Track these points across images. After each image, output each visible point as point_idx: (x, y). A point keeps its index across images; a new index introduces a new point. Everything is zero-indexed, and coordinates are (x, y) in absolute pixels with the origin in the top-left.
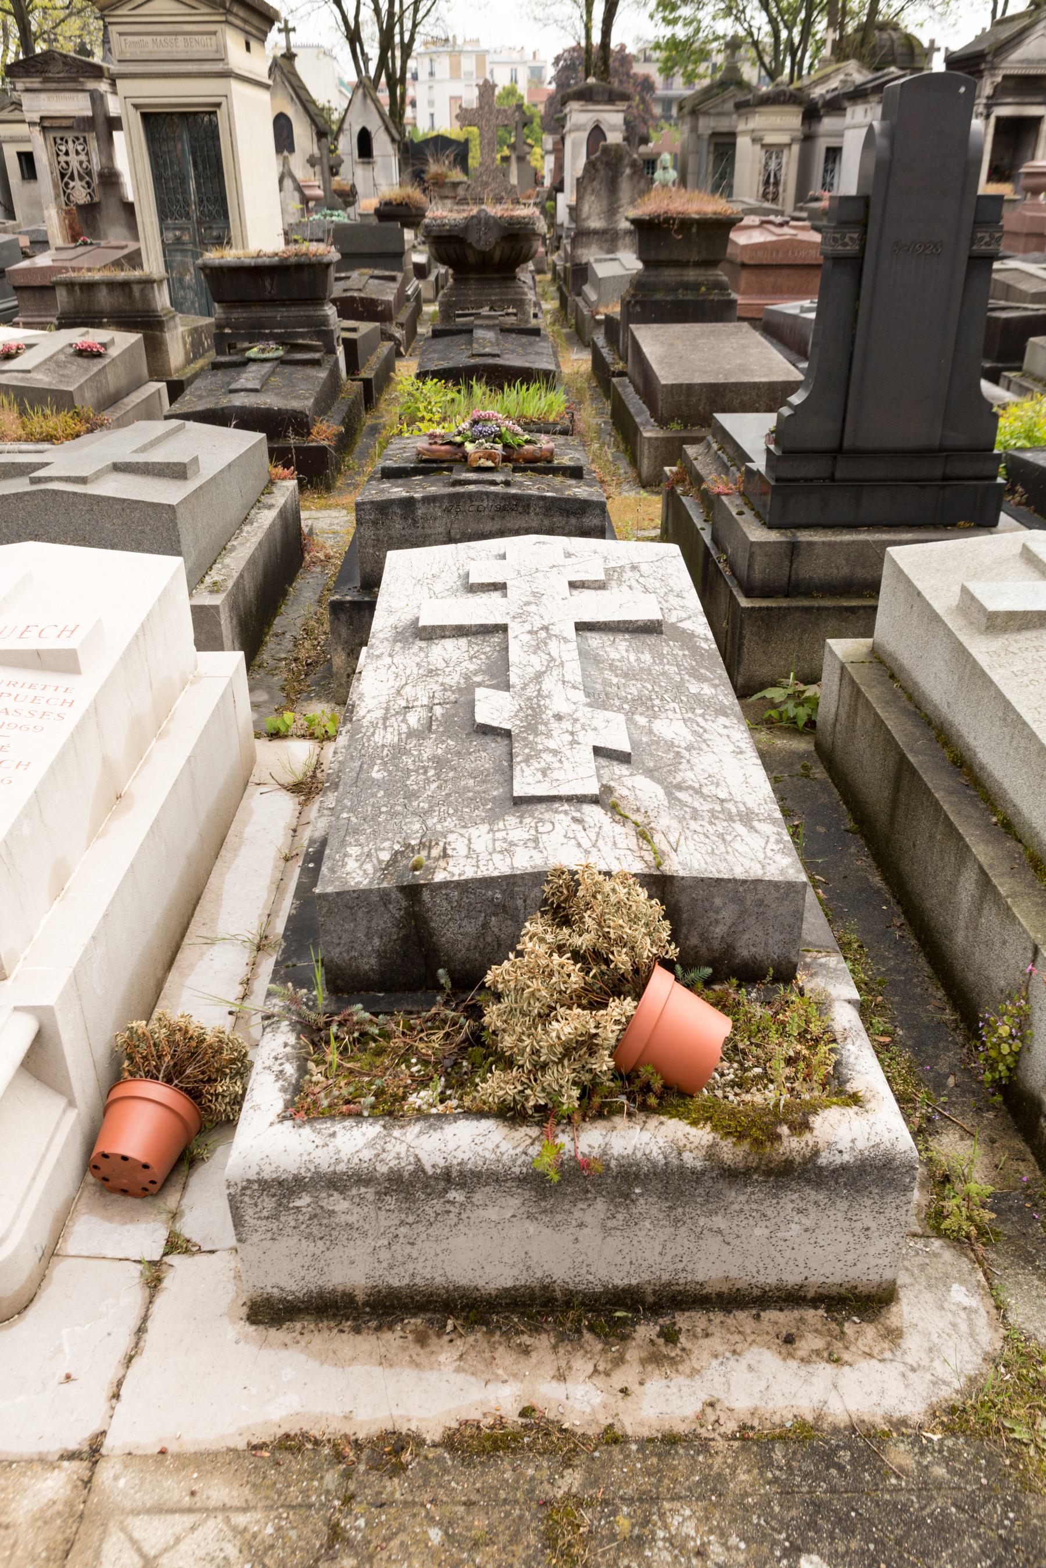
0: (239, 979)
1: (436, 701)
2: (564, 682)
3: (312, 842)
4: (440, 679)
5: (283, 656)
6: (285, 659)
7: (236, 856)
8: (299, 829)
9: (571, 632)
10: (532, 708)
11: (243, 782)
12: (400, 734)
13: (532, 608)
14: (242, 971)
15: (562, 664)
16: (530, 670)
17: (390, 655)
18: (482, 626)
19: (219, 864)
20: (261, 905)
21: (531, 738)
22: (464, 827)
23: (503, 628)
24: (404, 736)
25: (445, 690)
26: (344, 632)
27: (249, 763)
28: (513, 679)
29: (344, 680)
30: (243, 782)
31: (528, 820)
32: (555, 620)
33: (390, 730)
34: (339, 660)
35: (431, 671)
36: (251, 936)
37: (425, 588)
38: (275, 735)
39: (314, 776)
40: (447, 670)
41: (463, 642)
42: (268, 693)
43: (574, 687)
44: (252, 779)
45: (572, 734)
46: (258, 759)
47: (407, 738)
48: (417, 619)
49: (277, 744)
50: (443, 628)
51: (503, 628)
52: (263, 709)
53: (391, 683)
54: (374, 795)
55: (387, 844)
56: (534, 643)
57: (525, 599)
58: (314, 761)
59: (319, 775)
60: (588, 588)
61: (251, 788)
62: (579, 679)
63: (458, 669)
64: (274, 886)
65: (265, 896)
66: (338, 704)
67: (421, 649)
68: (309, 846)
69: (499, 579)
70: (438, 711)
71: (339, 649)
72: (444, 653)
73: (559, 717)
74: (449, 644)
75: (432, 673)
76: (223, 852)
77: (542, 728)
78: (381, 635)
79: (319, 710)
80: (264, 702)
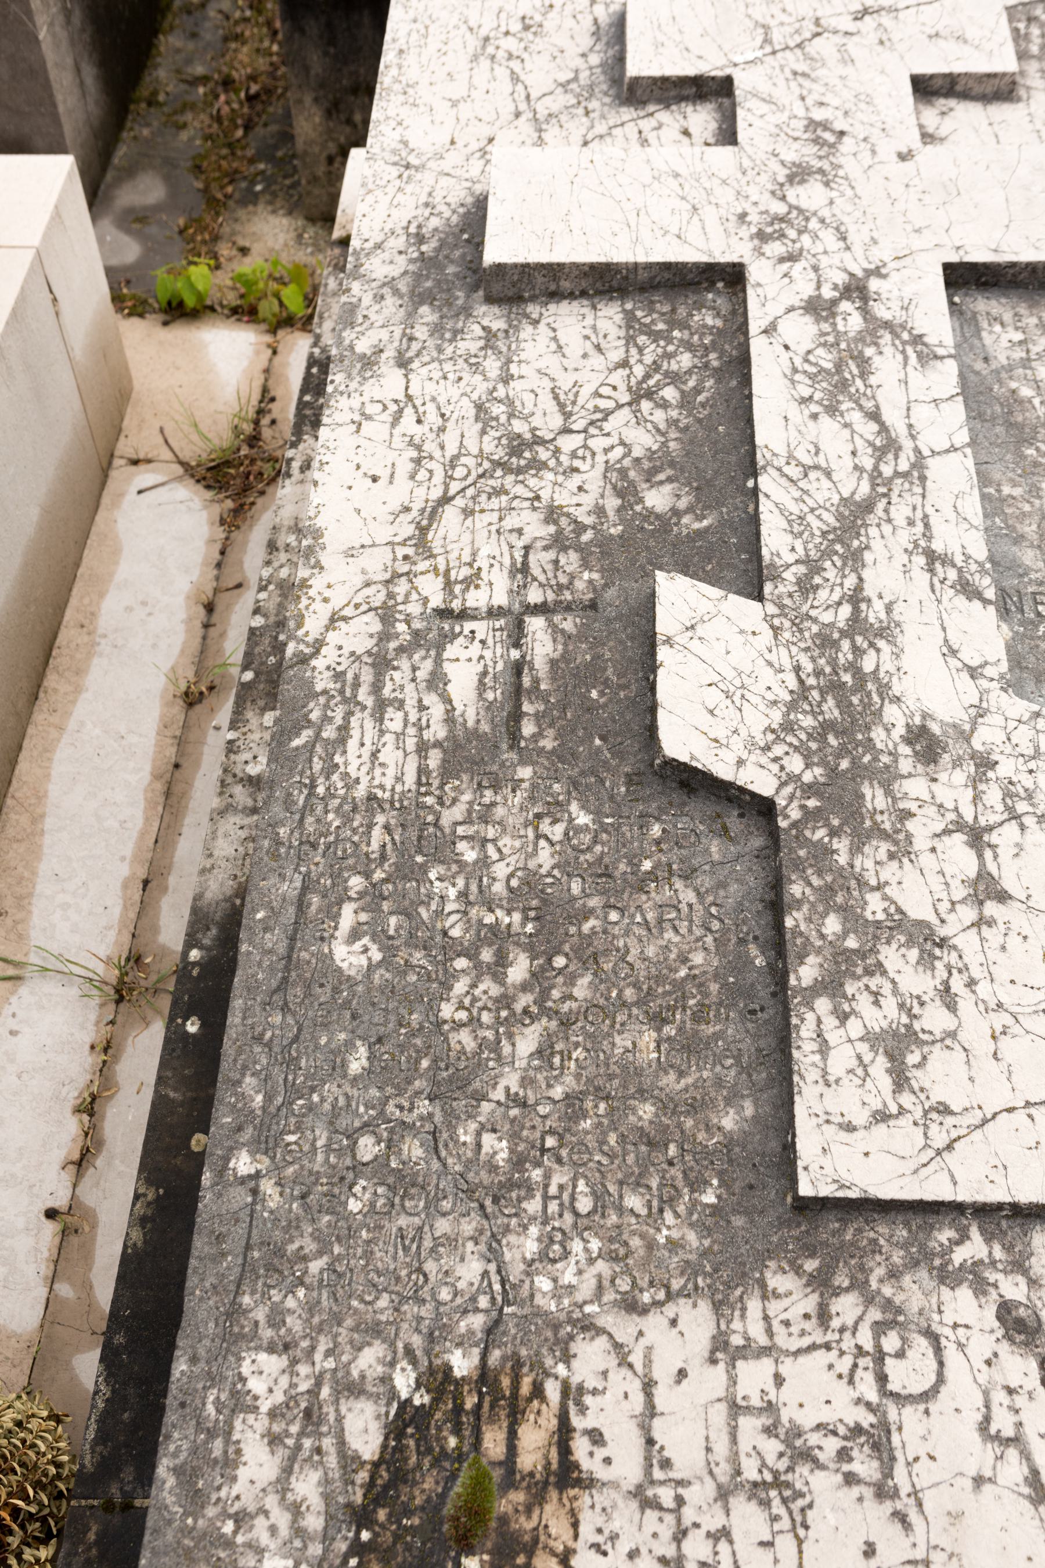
0: (71, 1102)
1: (535, 596)
2: (932, 558)
3: (198, 919)
4: (544, 484)
5: (199, 70)
6: (204, 80)
7: (78, 690)
8: (223, 599)
9: (933, 315)
10: (835, 687)
11: (99, 464)
12: (422, 748)
13: (810, 195)
14: (78, 1069)
15: (919, 464)
16: (821, 491)
17: (403, 362)
18: (667, 266)
19: (40, 716)
20: (128, 850)
21: (842, 845)
22: (631, 1306)
23: (733, 277)
24: (434, 758)
25: (558, 543)
26: (316, 61)
27: (110, 403)
28: (776, 541)
29: (321, 170)
30: (99, 464)
31: (846, 1307)
32: (882, 253)
33: (394, 721)
34: (308, 124)
35: (517, 445)
36: (100, 968)
37: (502, 73)
38: (178, 311)
39: (254, 440)
40: (569, 443)
41: (609, 317)
42: (167, 179)
43: (968, 590)
44: (125, 448)
45: (977, 837)
46: (136, 384)
47: (447, 772)
48: (475, 219)
49: (181, 333)
50: (553, 270)
51: (733, 277)
52: (153, 230)
53: (400, 492)
54: (337, 1067)
55: (369, 1360)
56: (825, 359)
57: (790, 155)
58: (256, 396)
59: (266, 433)
60: (966, 95)
61: (119, 472)
62: (980, 551)
63: (598, 443)
64: (160, 786)
65: (139, 822)
66: (311, 220)
67: (489, 335)
68: (189, 945)
69: (710, 66)
70: (541, 642)
71: (308, 99)
72: (552, 363)
73: (926, 745)
74: (568, 320)
75: (522, 453)
76: (51, 680)
77: (874, 797)
78: (378, 268)
79: (270, 235)
80: (157, 208)
